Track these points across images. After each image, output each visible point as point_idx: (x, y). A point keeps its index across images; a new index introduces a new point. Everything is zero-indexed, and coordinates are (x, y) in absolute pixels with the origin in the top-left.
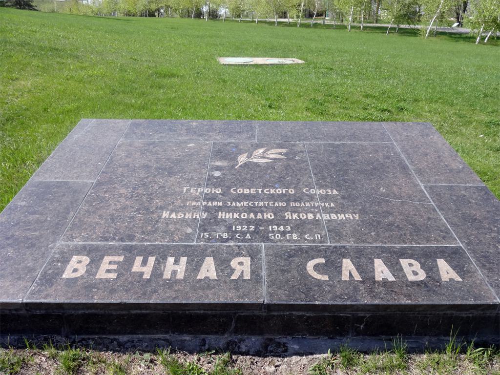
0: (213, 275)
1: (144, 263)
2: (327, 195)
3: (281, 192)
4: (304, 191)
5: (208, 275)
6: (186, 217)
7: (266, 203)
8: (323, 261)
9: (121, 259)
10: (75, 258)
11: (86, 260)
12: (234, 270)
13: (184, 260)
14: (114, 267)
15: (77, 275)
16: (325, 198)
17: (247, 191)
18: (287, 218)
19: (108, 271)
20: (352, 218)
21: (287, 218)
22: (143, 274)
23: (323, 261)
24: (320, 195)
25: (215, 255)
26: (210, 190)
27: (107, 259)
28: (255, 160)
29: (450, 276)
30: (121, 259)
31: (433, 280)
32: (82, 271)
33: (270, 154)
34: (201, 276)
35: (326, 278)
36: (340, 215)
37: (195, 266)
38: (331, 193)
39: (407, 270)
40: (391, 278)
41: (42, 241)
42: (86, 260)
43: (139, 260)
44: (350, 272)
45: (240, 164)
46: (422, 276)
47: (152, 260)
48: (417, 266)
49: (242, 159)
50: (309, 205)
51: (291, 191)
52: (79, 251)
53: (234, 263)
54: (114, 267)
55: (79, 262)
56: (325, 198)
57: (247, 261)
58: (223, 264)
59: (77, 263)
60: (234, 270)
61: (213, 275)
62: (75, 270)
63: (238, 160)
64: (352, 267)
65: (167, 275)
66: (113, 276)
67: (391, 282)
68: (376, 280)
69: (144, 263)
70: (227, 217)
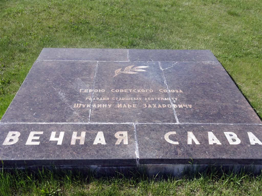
0: (103, 142)
1: (57, 136)
2: (175, 93)
3: (118, 91)
4: (160, 90)
5: (99, 142)
6: (98, 107)
7: (117, 98)
8: (174, 133)
9: (42, 133)
10: (11, 133)
11: (18, 134)
12: (117, 139)
13: (83, 134)
14: (38, 138)
15: (12, 143)
16: (175, 95)
17: (104, 99)
18: (118, 143)
19: (33, 140)
20: (187, 107)
21: (118, 143)
22: (57, 142)
23: (174, 133)
24: (171, 93)
25: (104, 129)
26: (97, 90)
27: (32, 133)
28: (126, 72)
29: (214, 142)
30: (42, 133)
31: (183, 144)
32: (16, 140)
33: (136, 69)
34: (95, 143)
35: (177, 143)
36: (181, 107)
37: (90, 137)
38: (178, 92)
39: (229, 139)
40: (219, 143)
41: (104, 57)
42: (18, 134)
43: (53, 134)
44: (192, 140)
45: (116, 75)
46: (238, 142)
47: (62, 134)
48: (235, 136)
49: (118, 72)
50: (154, 100)
51: (143, 91)
52: (14, 129)
53: (117, 135)
54: (38, 138)
55: (14, 135)
56: (175, 95)
57: (125, 133)
58: (110, 138)
59: (34, 136)
60: (117, 139)
61: (103, 142)
62: (11, 140)
63: (115, 72)
64: (194, 137)
65: (73, 143)
66: (38, 143)
67: (219, 145)
68: (127, 132)
69: (57, 136)
70: (103, 107)
